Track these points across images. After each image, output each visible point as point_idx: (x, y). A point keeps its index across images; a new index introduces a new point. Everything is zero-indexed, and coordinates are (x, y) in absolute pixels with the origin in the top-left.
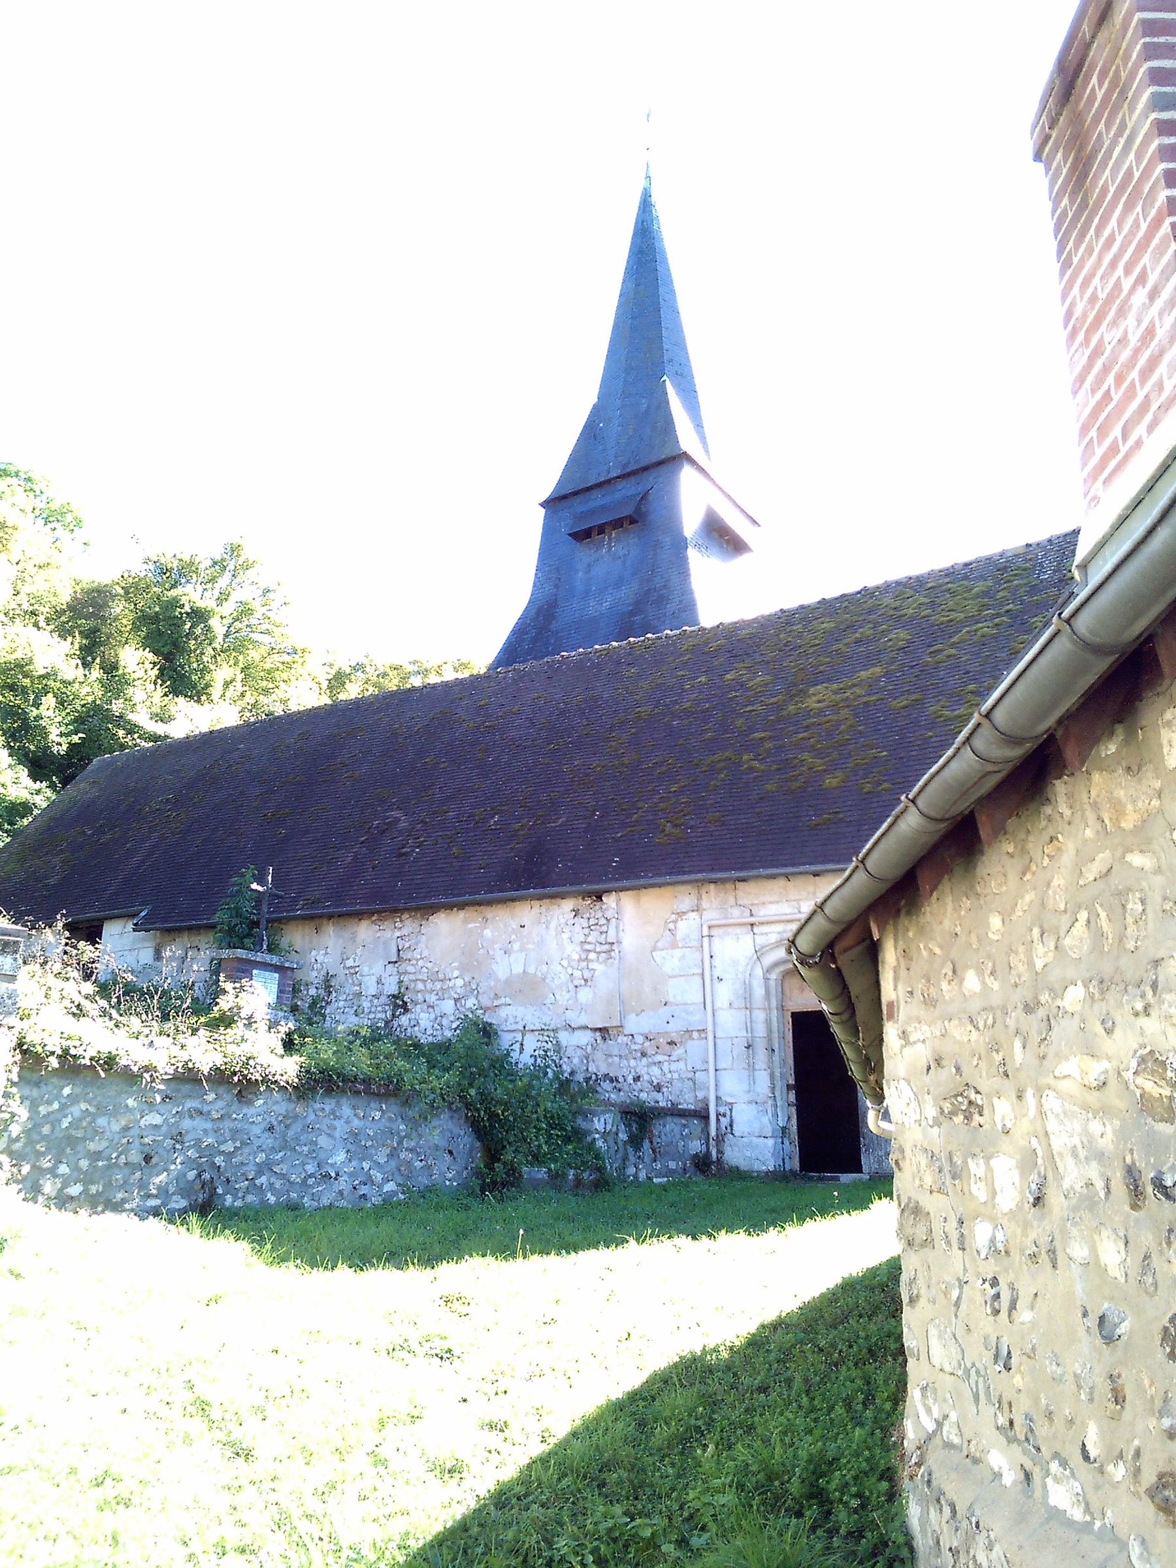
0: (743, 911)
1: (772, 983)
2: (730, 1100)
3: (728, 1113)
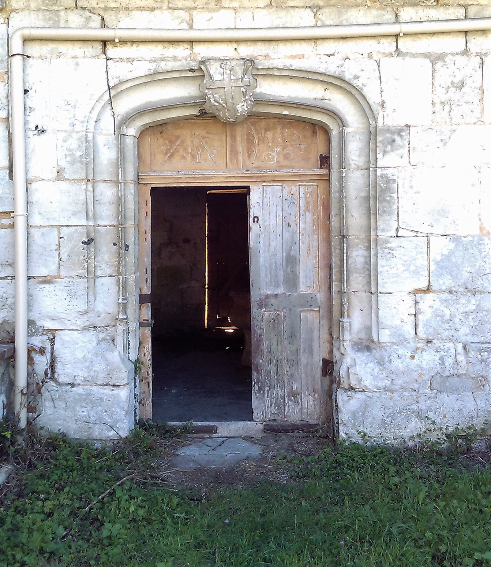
0: (88, 19)
1: (130, 142)
2: (50, 325)
3: (48, 346)
